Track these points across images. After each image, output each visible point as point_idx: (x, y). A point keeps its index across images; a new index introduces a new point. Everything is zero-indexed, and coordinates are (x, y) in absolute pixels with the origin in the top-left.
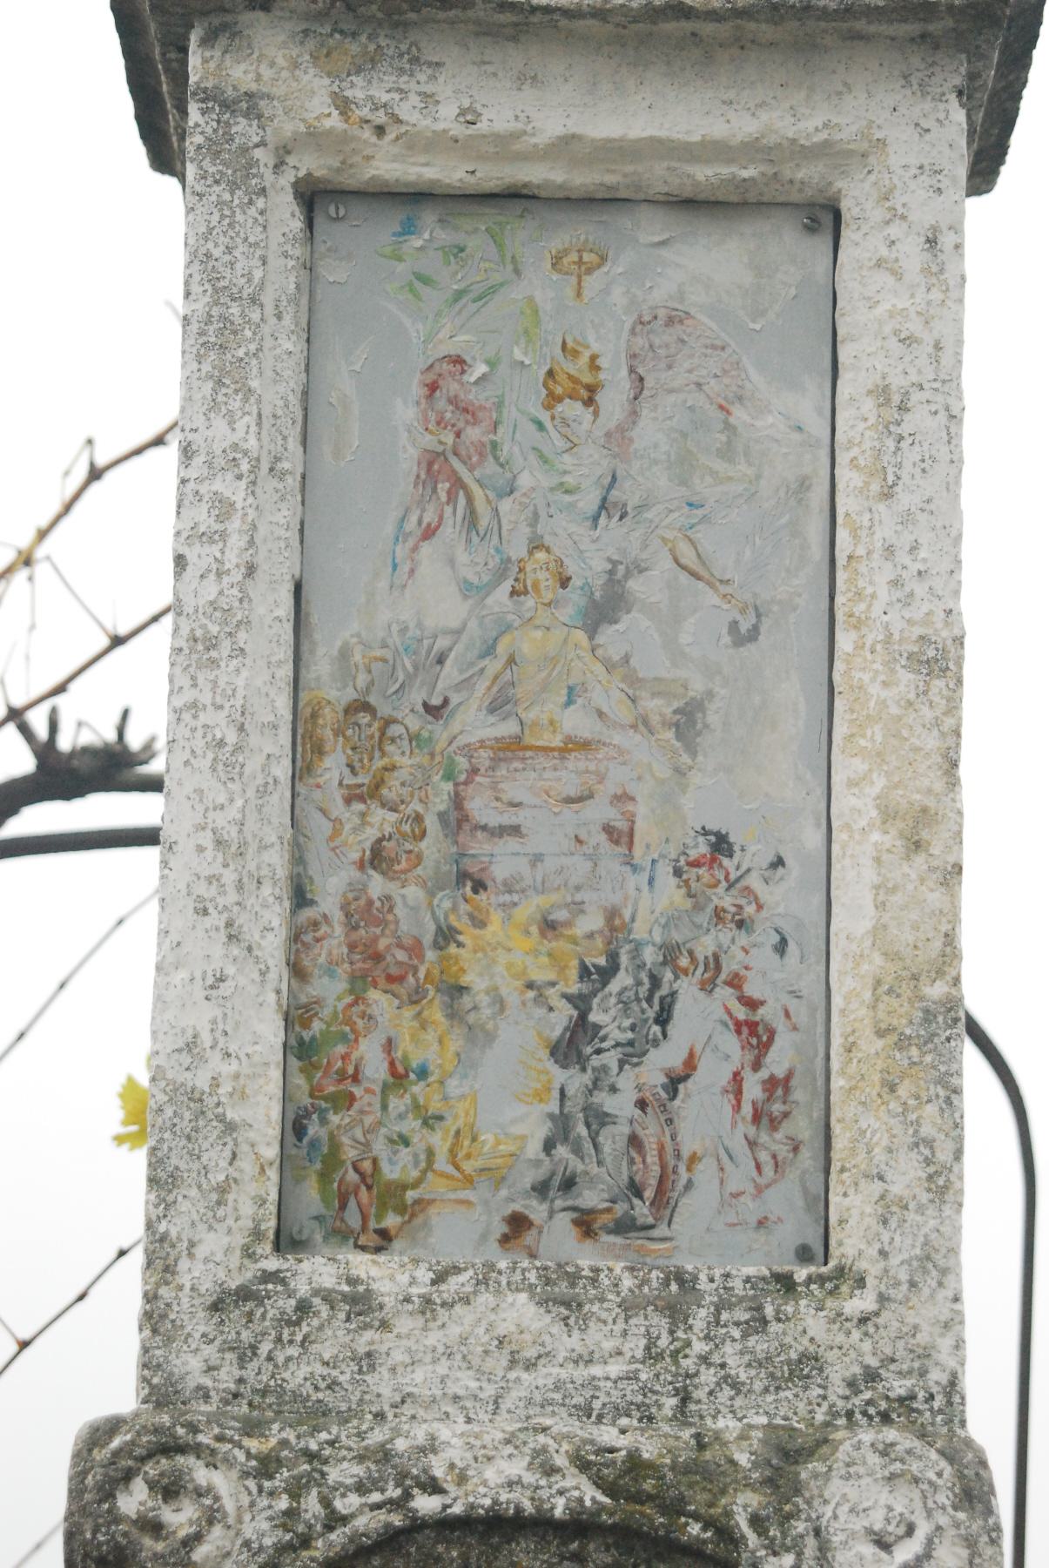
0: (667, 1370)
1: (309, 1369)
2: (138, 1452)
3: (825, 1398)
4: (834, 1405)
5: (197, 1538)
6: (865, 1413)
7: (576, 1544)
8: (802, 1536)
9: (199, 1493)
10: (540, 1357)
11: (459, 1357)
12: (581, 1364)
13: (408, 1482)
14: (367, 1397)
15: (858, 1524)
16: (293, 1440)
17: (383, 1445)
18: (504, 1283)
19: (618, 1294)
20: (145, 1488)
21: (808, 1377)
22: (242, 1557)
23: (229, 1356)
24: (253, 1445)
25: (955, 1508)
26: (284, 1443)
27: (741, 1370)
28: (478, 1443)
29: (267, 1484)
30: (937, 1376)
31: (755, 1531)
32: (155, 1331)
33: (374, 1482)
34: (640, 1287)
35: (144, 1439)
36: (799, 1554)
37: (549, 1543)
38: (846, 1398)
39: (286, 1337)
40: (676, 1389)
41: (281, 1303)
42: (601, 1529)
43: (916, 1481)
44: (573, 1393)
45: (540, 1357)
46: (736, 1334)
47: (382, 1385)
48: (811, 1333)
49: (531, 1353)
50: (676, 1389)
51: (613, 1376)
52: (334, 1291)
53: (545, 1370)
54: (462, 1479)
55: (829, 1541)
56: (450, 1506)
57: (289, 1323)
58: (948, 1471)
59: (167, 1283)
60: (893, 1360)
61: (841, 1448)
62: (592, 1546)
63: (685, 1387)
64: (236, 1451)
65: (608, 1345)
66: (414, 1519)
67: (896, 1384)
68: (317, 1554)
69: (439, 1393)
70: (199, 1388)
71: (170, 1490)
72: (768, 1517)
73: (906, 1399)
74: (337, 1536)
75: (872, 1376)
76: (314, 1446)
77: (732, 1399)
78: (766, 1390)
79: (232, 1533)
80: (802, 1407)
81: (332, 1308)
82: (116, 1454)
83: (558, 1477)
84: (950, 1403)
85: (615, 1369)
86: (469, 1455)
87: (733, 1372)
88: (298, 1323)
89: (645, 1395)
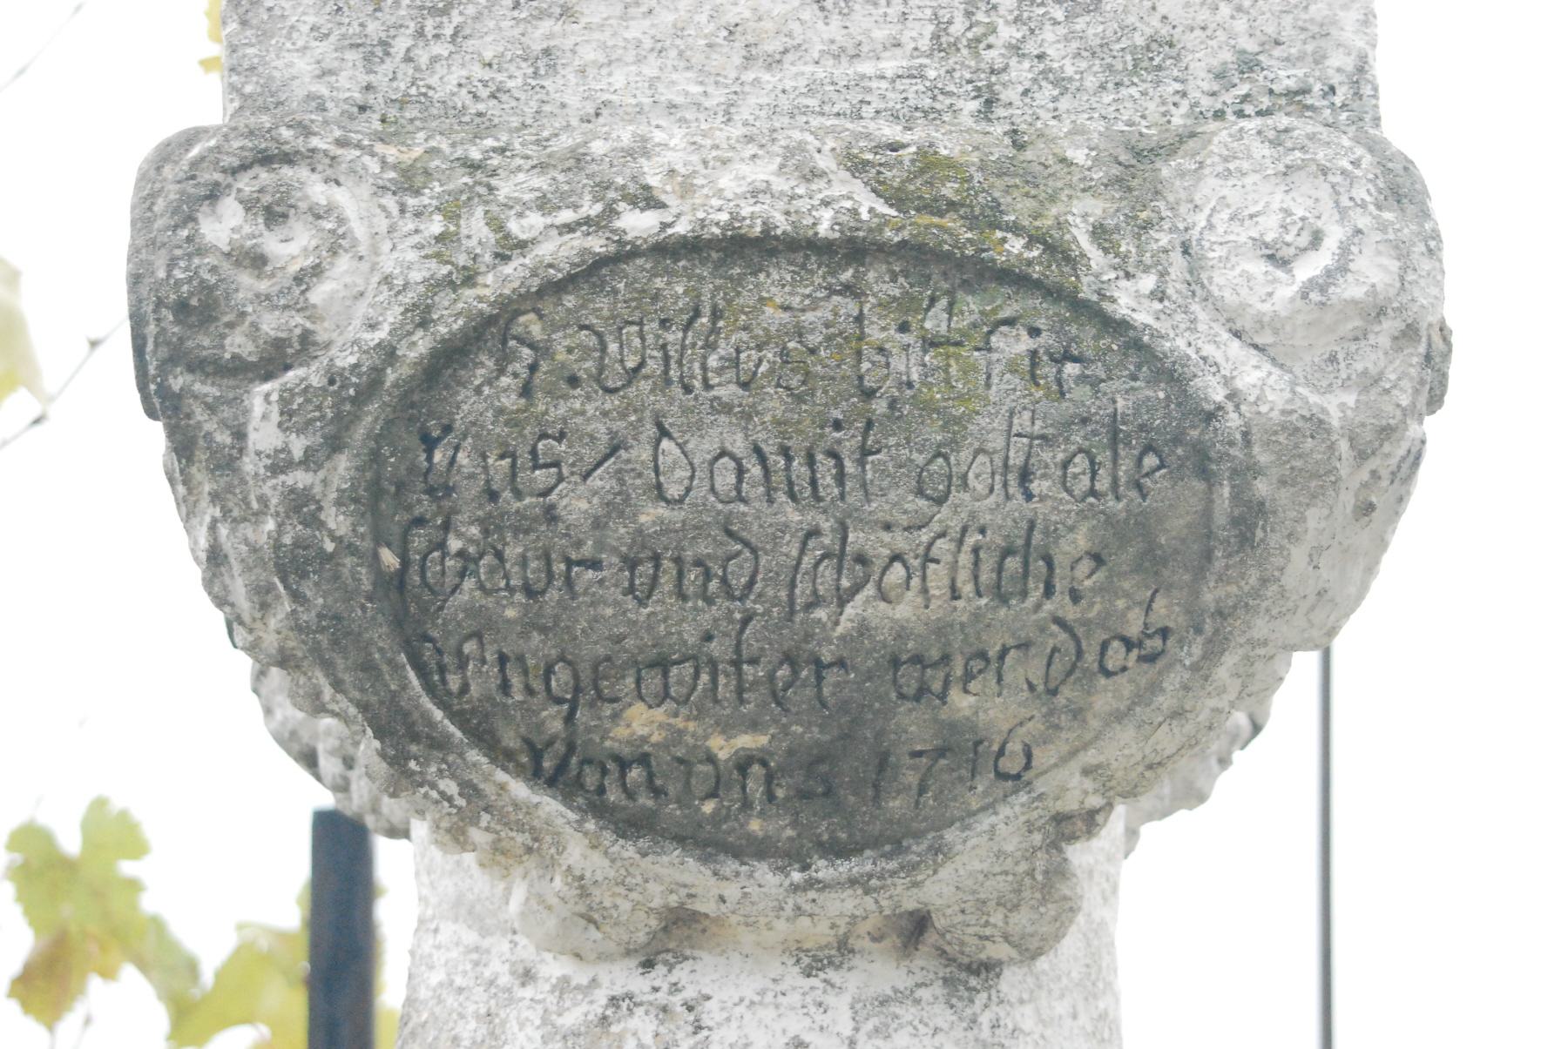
1: (464, 73)
2: (229, 161)
3: (1184, 94)
4: (1196, 104)
5: (317, 271)
8: (1166, 251)
9: (317, 214)
10: (786, 51)
11: (673, 53)
12: (844, 59)
13: (611, 194)
14: (547, 108)
15: (1243, 235)
16: (445, 146)
17: (573, 150)
20: (239, 210)
21: (1159, 68)
22: (381, 298)
23: (352, 56)
24: (391, 152)
25: (1379, 207)
26: (433, 152)
27: (1067, 62)
28: (708, 142)
29: (411, 202)
30: (1338, 61)
32: (244, 23)
33: (563, 196)
35: (236, 144)
36: (1163, 275)
37: (812, 272)
38: (1213, 94)
39: (429, 30)
40: (978, 89)
42: (883, 250)
43: (1324, 171)
44: (835, 96)
45: (786, 51)
47: (567, 90)
49: (773, 46)
51: (889, 74)
53: (794, 69)
54: (687, 189)
55: (1203, 258)
56: (670, 225)
58: (1367, 160)
60: (1277, 43)
61: (1216, 140)
62: (871, 275)
64: (367, 159)
65: (880, 34)
67: (1282, 73)
68: (487, 292)
69: (647, 101)
70: (310, 97)
71: (274, 215)
72: (1117, 229)
73: (1297, 93)
74: (515, 269)
75: (1248, 65)
76: (475, 155)
77: (1055, 100)
78: (1103, 87)
79: (365, 266)
80: (1152, 107)
82: (195, 164)
83: (822, 183)
84: (1358, 95)
85: (890, 66)
86: (695, 158)
87: (1055, 65)
89: (934, 98)
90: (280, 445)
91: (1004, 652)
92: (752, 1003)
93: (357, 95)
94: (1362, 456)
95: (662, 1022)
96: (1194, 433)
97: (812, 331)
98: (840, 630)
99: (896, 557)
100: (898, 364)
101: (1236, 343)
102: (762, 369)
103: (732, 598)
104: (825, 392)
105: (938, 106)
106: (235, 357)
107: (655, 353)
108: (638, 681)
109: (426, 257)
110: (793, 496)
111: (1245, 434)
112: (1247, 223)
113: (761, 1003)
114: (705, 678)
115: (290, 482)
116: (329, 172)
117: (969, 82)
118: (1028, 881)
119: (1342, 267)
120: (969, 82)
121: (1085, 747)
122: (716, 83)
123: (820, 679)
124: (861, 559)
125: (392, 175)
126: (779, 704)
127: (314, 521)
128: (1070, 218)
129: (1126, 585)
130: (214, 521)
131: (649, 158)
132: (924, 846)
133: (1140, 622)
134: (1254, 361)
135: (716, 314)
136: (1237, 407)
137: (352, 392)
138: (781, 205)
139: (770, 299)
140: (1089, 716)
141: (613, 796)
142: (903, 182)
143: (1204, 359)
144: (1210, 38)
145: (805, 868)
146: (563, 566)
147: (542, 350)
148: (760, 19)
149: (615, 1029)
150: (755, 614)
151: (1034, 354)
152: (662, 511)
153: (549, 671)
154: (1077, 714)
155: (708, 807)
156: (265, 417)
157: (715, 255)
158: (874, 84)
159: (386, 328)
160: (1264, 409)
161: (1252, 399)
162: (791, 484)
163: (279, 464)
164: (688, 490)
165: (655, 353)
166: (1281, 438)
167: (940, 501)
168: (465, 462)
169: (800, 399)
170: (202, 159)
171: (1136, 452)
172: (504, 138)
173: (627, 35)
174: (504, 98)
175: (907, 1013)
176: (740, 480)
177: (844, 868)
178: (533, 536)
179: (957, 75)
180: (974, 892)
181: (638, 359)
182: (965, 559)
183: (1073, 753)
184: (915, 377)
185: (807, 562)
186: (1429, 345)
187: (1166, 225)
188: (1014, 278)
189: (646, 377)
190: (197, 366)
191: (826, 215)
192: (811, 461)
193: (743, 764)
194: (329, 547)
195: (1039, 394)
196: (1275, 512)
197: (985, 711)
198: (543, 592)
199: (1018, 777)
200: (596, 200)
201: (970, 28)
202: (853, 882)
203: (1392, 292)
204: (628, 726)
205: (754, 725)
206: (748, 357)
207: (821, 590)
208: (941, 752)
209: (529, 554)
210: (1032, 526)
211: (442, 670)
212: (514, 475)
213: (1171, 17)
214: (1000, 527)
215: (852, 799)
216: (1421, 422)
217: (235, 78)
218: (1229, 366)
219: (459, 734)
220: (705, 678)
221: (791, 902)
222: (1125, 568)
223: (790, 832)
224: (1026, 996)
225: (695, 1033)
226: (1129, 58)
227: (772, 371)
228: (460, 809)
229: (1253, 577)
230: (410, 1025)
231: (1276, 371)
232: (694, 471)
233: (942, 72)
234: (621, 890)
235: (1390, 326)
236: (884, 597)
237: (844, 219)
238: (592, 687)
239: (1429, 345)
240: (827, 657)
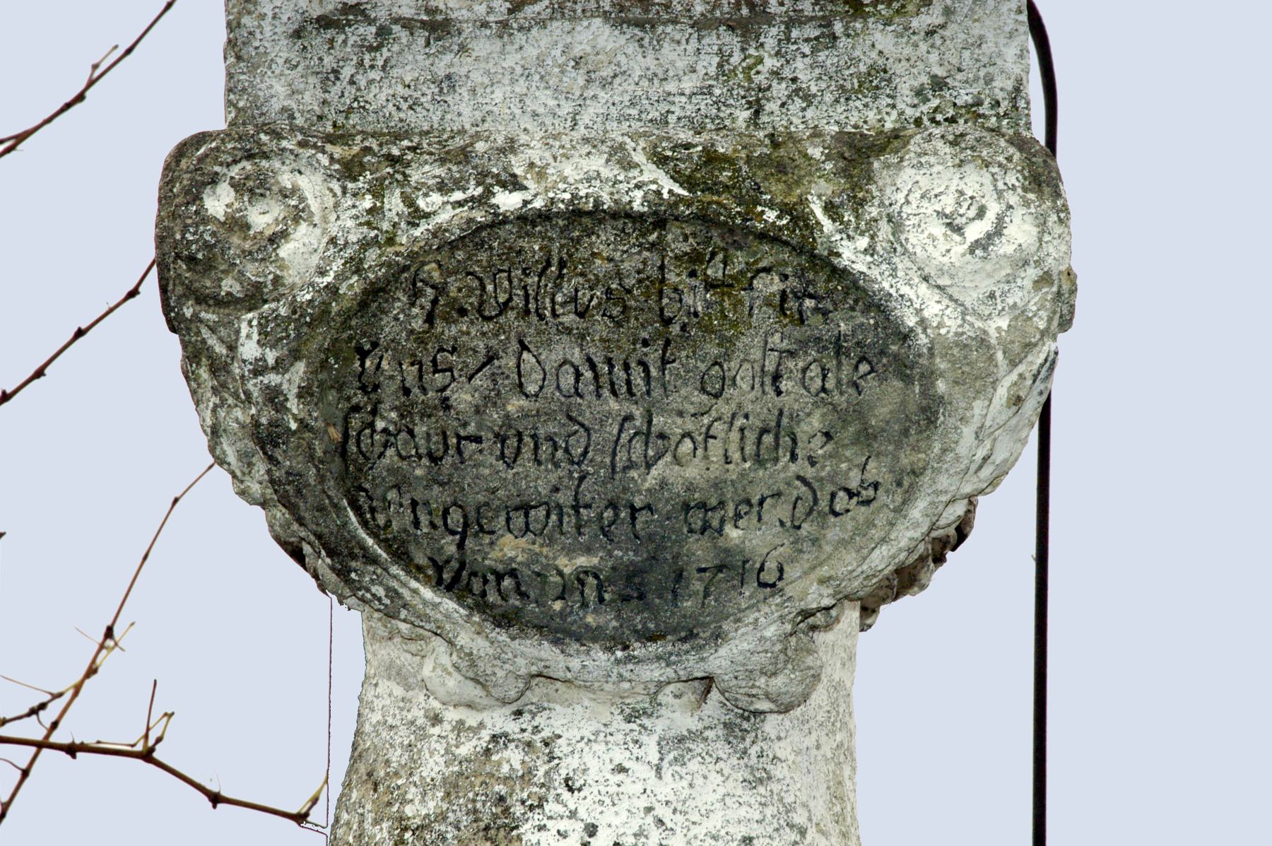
0: (739, 85)
1: (391, 92)
3: (894, 106)
6: (933, 120)
7: (655, 235)
8: (876, 221)
9: (284, 194)
10: (615, 76)
11: (537, 77)
13: (489, 180)
16: (376, 148)
18: (579, 11)
19: (691, 18)
21: (877, 88)
22: (328, 253)
23: (312, 80)
24: (337, 151)
26: (367, 150)
27: (812, 83)
29: (350, 185)
31: (830, 217)
32: (239, 58)
34: (712, 11)
35: (229, 146)
38: (915, 106)
39: (367, 63)
40: (749, 102)
41: (361, 30)
44: (649, 107)
46: (806, 49)
48: (879, 47)
49: (607, 72)
50: (749, 102)
51: (687, 92)
52: (413, 19)
54: (541, 175)
57: (371, 49)
59: (249, 13)
60: (960, 70)
61: (912, 142)
62: (670, 237)
63: (758, 100)
64: (320, 155)
66: (496, 215)
67: (963, 92)
68: (402, 249)
71: (253, 188)
73: (972, 106)
75: (939, 84)
76: (395, 152)
77: (804, 110)
78: (837, 101)
79: (318, 231)
81: (412, 34)
82: (200, 160)
84: (1015, 107)
85: (689, 84)
88: (378, 48)
89: (719, 109)
90: (258, 355)
91: (761, 503)
92: (589, 740)
93: (316, 108)
94: (1013, 364)
95: (526, 753)
96: (894, 348)
97: (628, 277)
98: (647, 485)
99: (687, 435)
100: (688, 299)
101: (924, 285)
102: (593, 303)
103: (573, 463)
104: (637, 319)
105: (722, 115)
106: (229, 294)
107: (518, 292)
108: (508, 520)
109: (361, 224)
110: (614, 393)
111: (930, 349)
112: (933, 200)
113: (595, 741)
114: (554, 517)
115: (266, 382)
116: (294, 165)
117: (743, 97)
118: (782, 657)
119: (998, 230)
120: (743, 97)
121: (821, 564)
122: (567, 98)
123: (633, 518)
124: (662, 436)
125: (337, 167)
126: (605, 535)
127: (281, 408)
128: (809, 197)
129: (848, 453)
130: (216, 406)
131: (516, 155)
132: (707, 634)
133: (858, 479)
134: (937, 298)
135: (562, 264)
136: (925, 330)
137: (308, 319)
138: (608, 189)
139: (599, 254)
140: (823, 542)
141: (492, 597)
142: (693, 171)
143: (902, 296)
144: (913, 67)
145: (625, 648)
146: (455, 440)
147: (440, 289)
148: (598, 54)
149: (494, 758)
150: (588, 473)
151: (783, 293)
152: (523, 402)
153: (446, 512)
154: (815, 541)
155: (558, 606)
156: (248, 336)
157: (561, 223)
158: (677, 99)
159: (332, 274)
160: (943, 331)
161: (935, 324)
162: (612, 384)
163: (259, 369)
164: (541, 388)
165: (518, 292)
166: (955, 351)
167: (717, 396)
168: (387, 367)
169: (619, 325)
170: (207, 156)
171: (854, 362)
172: (416, 139)
173: (504, 65)
174: (419, 109)
175: (699, 748)
176: (577, 380)
177: (652, 648)
178: (433, 419)
179: (735, 92)
180: (744, 665)
181: (507, 296)
182: (735, 435)
183: (813, 568)
184: (700, 309)
185: (625, 437)
186: (1060, 286)
187: (876, 202)
188: (769, 236)
189: (512, 309)
190: (201, 300)
191: (638, 194)
192: (626, 367)
193: (581, 577)
194: (294, 426)
195: (786, 321)
196: (950, 403)
197: (750, 540)
198: (441, 459)
199: (773, 585)
200: (478, 184)
201: (744, 60)
202: (659, 658)
203: (1034, 249)
204: (501, 550)
205: (588, 550)
206: (584, 296)
207: (634, 459)
208: (720, 568)
209: (432, 431)
210: (781, 413)
211: (373, 510)
212: (421, 377)
213: (886, 52)
214: (758, 414)
215: (657, 601)
216: (1055, 339)
217: (232, 96)
218: (919, 301)
219: (384, 555)
220: (554, 517)
221: (615, 671)
222: (846, 442)
223: (615, 623)
224: (783, 735)
225: (549, 761)
226: (855, 81)
227: (600, 304)
228: (386, 606)
229: (937, 447)
230: (359, 749)
231: (952, 304)
232: (545, 374)
233: (725, 90)
234: (498, 662)
235: (1032, 273)
236: (677, 460)
237: (651, 197)
238: (475, 524)
239: (1060, 286)
240: (638, 504)
